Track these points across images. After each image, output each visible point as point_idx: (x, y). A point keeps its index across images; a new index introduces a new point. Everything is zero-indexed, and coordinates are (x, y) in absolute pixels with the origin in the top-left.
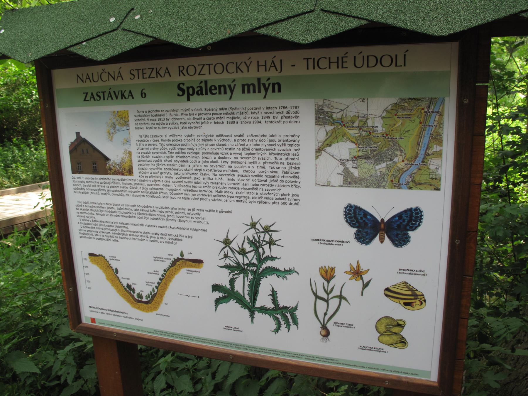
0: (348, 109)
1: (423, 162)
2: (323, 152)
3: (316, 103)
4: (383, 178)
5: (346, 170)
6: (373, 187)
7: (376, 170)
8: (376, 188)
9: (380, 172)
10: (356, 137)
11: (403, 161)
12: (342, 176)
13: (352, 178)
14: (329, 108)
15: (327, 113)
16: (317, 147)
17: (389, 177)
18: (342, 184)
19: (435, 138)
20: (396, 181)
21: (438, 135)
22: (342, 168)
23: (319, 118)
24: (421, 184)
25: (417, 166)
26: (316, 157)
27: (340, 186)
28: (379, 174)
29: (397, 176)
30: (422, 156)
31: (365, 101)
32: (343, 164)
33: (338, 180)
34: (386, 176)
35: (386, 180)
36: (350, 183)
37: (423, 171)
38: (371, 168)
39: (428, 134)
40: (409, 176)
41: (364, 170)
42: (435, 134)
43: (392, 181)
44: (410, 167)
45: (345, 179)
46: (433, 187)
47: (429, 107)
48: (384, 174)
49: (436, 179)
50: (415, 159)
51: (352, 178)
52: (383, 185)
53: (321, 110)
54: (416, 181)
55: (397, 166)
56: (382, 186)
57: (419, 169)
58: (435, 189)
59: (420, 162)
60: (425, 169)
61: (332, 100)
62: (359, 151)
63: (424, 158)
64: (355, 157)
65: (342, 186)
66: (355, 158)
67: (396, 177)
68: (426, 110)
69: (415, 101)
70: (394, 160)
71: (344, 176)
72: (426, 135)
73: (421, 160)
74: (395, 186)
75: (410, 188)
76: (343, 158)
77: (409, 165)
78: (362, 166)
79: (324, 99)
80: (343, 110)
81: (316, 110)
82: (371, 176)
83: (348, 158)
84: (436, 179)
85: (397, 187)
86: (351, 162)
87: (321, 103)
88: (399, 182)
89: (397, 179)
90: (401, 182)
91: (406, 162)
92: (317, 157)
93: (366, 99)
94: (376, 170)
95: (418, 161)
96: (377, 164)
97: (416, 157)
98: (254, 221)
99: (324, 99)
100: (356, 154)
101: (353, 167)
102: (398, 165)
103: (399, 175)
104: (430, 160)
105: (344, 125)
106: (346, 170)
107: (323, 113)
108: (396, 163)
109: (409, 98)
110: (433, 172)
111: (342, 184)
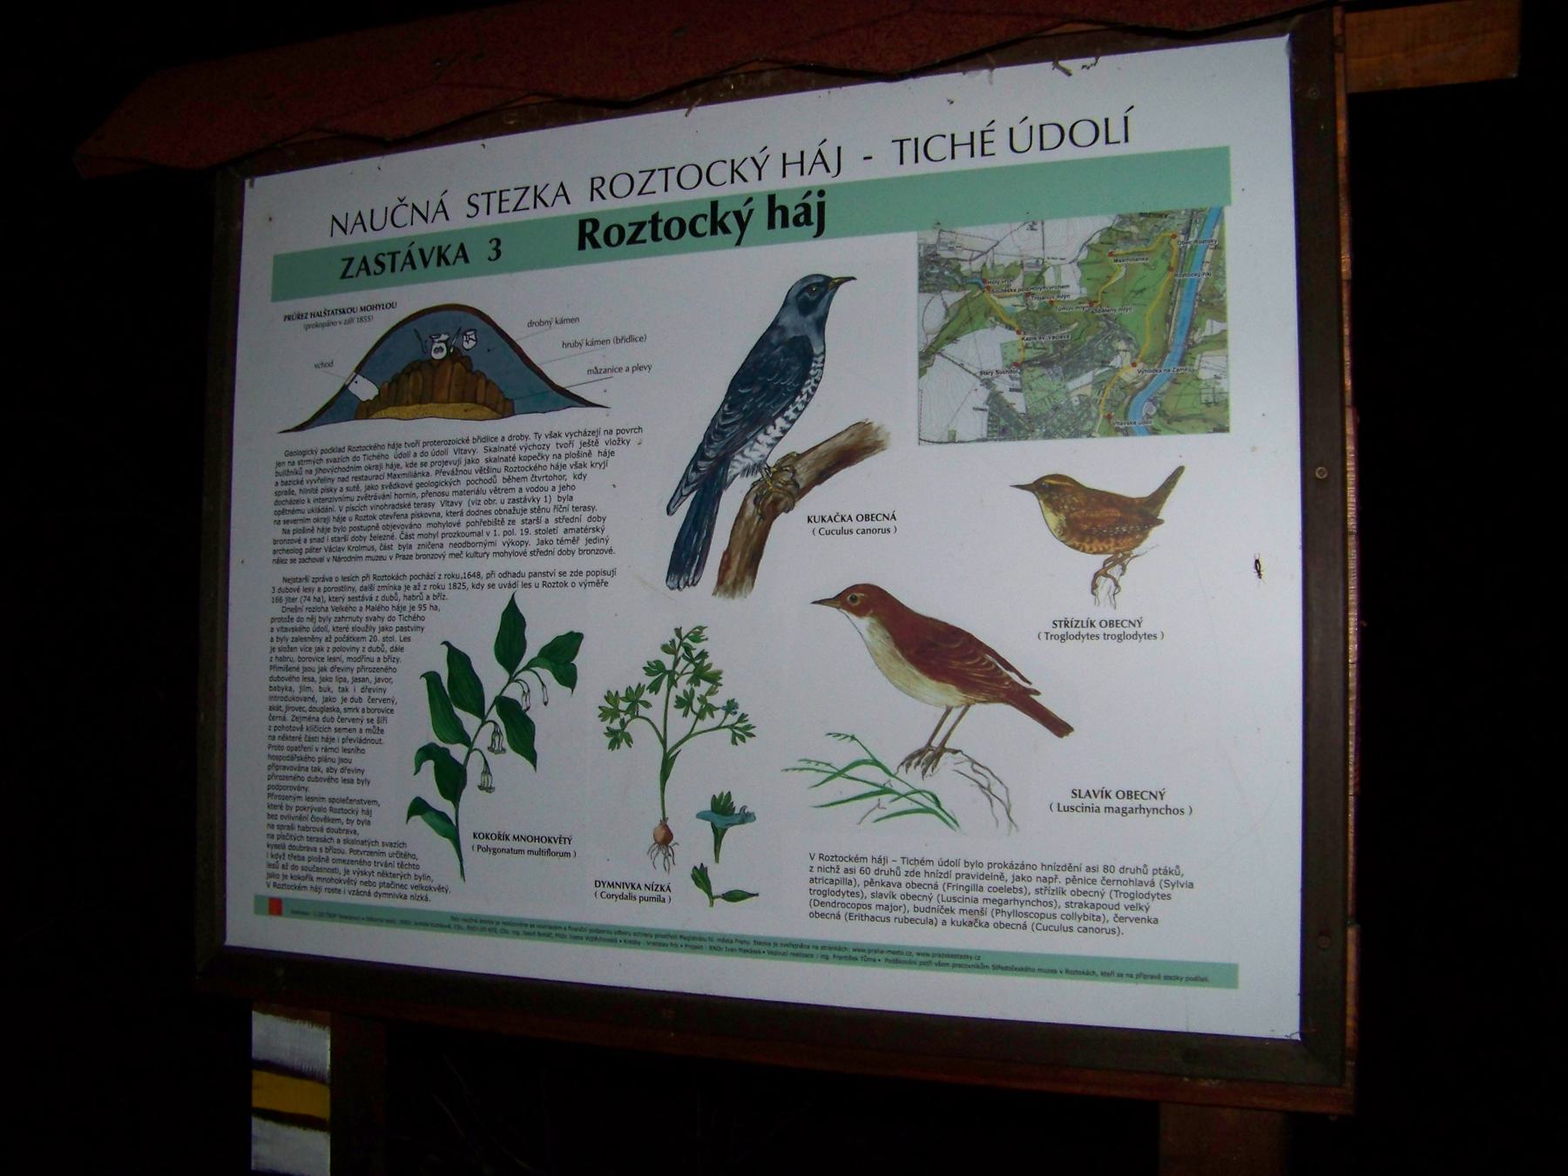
5: (995, 398)
7: (1068, 393)
11: (1134, 365)
14: (951, 249)
15: (948, 261)
16: (923, 348)
22: (984, 393)
28: (1075, 402)
30: (1180, 350)
31: (1038, 226)
32: (987, 384)
34: (1093, 408)
41: (1040, 395)
45: (993, 422)
48: (1088, 401)
49: (1216, 404)
50: (1163, 357)
52: (1086, 428)
57: (1175, 382)
58: (1215, 430)
64: (1016, 364)
65: (984, 440)
67: (1117, 407)
68: (1182, 238)
73: (1177, 358)
74: (1117, 430)
78: (1033, 385)
83: (1000, 368)
86: (1006, 377)
87: (931, 238)
89: (1122, 409)
91: (1140, 366)
100: (1019, 356)
102: (1122, 375)
106: (995, 398)
107: (937, 262)
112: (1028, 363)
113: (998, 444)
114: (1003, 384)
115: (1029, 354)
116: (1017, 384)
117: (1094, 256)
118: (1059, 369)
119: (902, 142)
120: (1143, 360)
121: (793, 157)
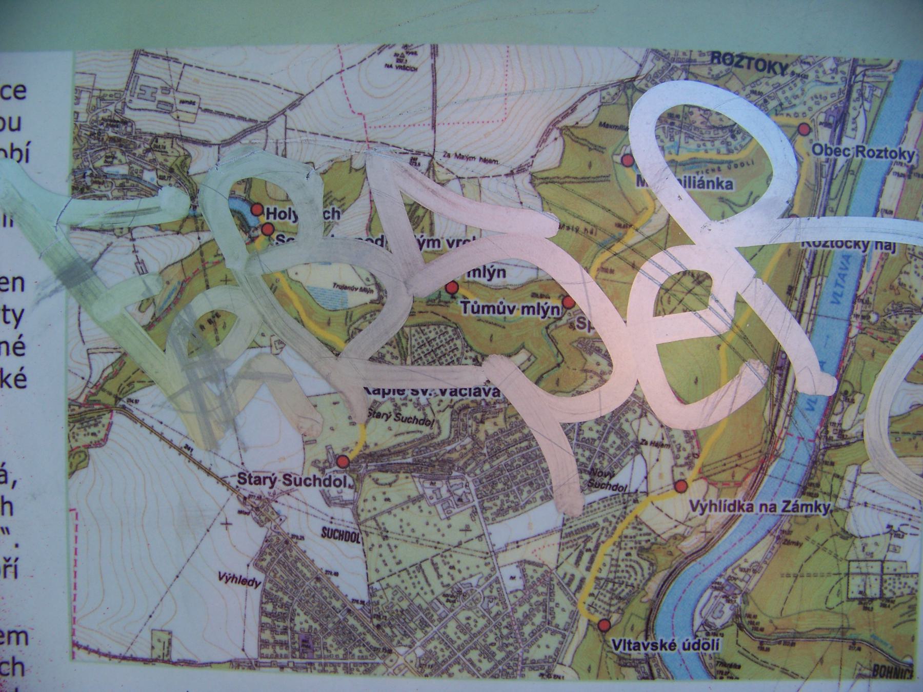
0: (296, 117)
1: (807, 487)
2: (119, 419)
3: (87, 82)
4: (546, 607)
5: (280, 550)
6: (473, 671)
7: (492, 554)
8: (492, 674)
9: (522, 563)
10: (349, 315)
11: (680, 486)
12: (255, 594)
13: (322, 612)
14: (166, 108)
15: (155, 143)
16: (76, 388)
17: (583, 597)
18: (253, 652)
19: (884, 327)
20: (628, 627)
21: (898, 309)
22: (249, 536)
23: (100, 178)
24: (790, 640)
25: (770, 520)
26: (72, 453)
27: (236, 664)
28: (508, 572)
29: (636, 590)
30: (804, 455)
31: (422, 60)
32: (258, 510)
33: (234, 621)
34: (560, 597)
35: (561, 619)
36: (306, 644)
37: (808, 548)
38: (454, 537)
39: (836, 298)
40: (716, 586)
41: (410, 554)
42: (881, 301)
43: (604, 627)
44: (727, 525)
45: (275, 615)
46: (863, 658)
47: (839, 121)
48: (547, 579)
49: (887, 602)
50: (761, 469)
51: (322, 612)
52: (537, 653)
53: (112, 123)
54: (763, 621)
55: (639, 523)
56: (534, 665)
57: (784, 539)
58: (878, 672)
59: (789, 492)
60: (819, 537)
61: (186, 55)
62: (374, 413)
63: (815, 462)
64: (341, 461)
65: (253, 665)
66: (346, 469)
67: (628, 600)
68: (824, 136)
69: (754, 75)
70: (621, 478)
71: (267, 596)
72: (826, 307)
73: (797, 474)
74: (624, 662)
75: (725, 670)
76: (253, 466)
77: (721, 516)
78: (391, 523)
79: (138, 54)
80: (266, 125)
81: (78, 126)
82: (455, 595)
83: (295, 467)
84: (887, 602)
85: (634, 664)
86: (312, 494)
87: (113, 78)
88: (648, 629)
89: (639, 608)
90: (662, 634)
91: (697, 490)
92: (78, 459)
93: (424, 52)
94: (492, 554)
95: (780, 484)
96: (502, 512)
97: (768, 455)
98: (596, 249)
99: (138, 54)
100: (350, 438)
101: (327, 533)
102: (646, 512)
103: (653, 586)
104: (851, 472)
105: (268, 230)
106: (280, 550)
107: (125, 146)
108: (628, 497)
109: (716, 57)
110: (870, 558)
111: (253, 652)
112: (379, 459)
113: (289, 676)
114: (304, 514)
115: (381, 435)
116: (344, 518)
117: (576, 164)
118: (465, 485)
119: (75, 644)
120: (703, 475)
121: (272, 210)
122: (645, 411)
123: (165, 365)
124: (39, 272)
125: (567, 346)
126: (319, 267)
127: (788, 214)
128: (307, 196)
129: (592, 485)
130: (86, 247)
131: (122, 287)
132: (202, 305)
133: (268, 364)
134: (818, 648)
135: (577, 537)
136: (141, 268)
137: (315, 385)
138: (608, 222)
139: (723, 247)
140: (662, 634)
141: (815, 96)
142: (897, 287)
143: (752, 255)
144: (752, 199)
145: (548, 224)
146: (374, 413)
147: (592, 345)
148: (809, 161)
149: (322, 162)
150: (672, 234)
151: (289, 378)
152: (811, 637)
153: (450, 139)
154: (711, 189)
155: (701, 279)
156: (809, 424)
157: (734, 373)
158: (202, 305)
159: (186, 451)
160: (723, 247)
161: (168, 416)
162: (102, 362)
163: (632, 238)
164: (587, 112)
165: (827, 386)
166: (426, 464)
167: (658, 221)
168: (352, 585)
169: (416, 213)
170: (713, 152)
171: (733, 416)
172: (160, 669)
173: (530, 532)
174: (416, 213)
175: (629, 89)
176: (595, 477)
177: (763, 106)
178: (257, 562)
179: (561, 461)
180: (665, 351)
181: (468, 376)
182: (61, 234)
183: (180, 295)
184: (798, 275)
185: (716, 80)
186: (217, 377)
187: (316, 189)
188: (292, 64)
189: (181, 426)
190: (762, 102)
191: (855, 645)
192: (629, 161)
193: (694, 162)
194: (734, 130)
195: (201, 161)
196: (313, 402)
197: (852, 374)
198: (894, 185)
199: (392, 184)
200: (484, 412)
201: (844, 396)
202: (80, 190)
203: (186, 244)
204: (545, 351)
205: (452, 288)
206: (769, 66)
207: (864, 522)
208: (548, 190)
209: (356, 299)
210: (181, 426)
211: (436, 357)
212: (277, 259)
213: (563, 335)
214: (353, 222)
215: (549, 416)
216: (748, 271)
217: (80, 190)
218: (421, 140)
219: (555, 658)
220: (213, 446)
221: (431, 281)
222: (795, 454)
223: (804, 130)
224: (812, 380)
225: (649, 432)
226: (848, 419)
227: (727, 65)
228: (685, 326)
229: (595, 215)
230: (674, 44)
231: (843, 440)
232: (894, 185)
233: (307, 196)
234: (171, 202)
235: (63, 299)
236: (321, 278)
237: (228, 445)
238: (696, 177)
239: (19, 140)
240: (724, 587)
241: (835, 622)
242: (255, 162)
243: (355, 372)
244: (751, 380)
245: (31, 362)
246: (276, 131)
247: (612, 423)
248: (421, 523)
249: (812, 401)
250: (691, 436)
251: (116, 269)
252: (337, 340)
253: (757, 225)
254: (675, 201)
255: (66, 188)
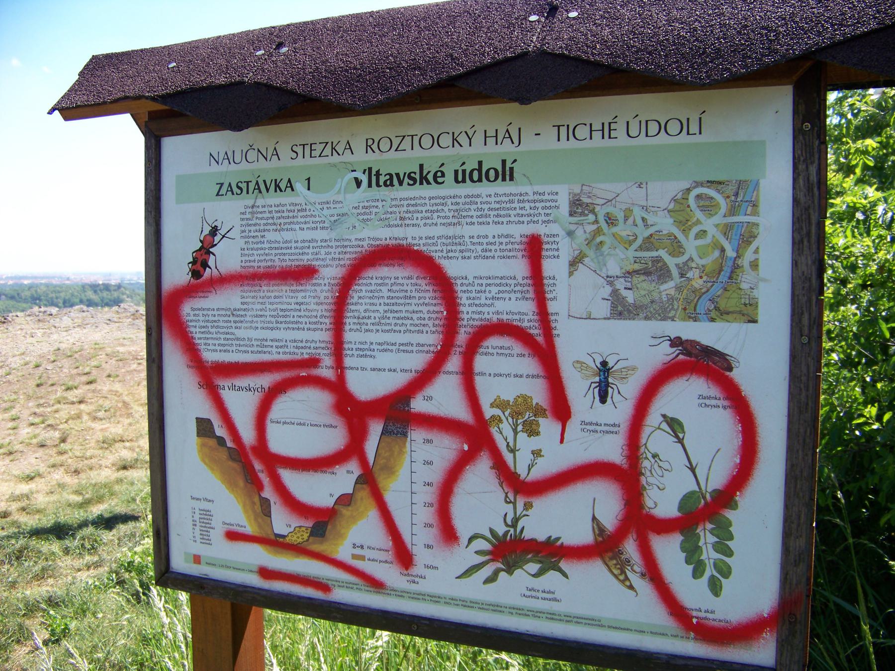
1: (730, 278)
5: (615, 293)
6: (657, 320)
7: (660, 292)
8: (661, 320)
11: (701, 277)
13: (624, 306)
14: (589, 197)
16: (571, 258)
20: (690, 309)
21: (751, 237)
22: (608, 289)
23: (575, 212)
24: (728, 313)
27: (605, 319)
29: (692, 301)
30: (729, 270)
31: (644, 186)
32: (611, 284)
33: (604, 308)
35: (676, 307)
36: (620, 314)
38: (652, 289)
41: (643, 293)
42: (746, 235)
43: (685, 309)
45: (614, 307)
47: (736, 195)
49: (751, 305)
50: (719, 273)
51: (624, 306)
52: (670, 315)
55: (692, 285)
56: (670, 318)
57: (725, 290)
58: (750, 321)
59: (726, 279)
61: (593, 185)
62: (635, 262)
63: (732, 272)
64: (628, 273)
65: (609, 319)
66: (630, 274)
68: (733, 198)
71: (612, 303)
72: (734, 237)
73: (728, 274)
74: (690, 317)
76: (610, 274)
77: (710, 284)
78: (639, 286)
82: (652, 302)
83: (618, 274)
84: (751, 305)
85: (692, 318)
86: (622, 280)
88: (695, 310)
89: (693, 305)
90: (698, 311)
91: (705, 278)
92: (571, 274)
94: (660, 292)
95: (724, 277)
97: (721, 270)
100: (630, 268)
101: (625, 288)
102: (693, 283)
105: (612, 223)
106: (615, 293)
108: (689, 280)
112: (636, 272)
114: (620, 284)
115: (637, 267)
117: (677, 208)
120: (706, 275)
122: (693, 261)
123: (591, 253)
124: (562, 233)
125: (677, 248)
126: (622, 230)
127: (725, 216)
128: (620, 216)
129: (682, 277)
130: (573, 227)
131: (581, 235)
132: (598, 240)
133: (613, 252)
134: (735, 315)
135: (679, 288)
136: (585, 232)
137: (623, 256)
138: (684, 220)
139: (711, 224)
140: (698, 311)
141: (730, 190)
142: (751, 232)
143: (717, 226)
144: (716, 213)
145: (671, 221)
146: (635, 262)
147: (681, 247)
148: (729, 204)
149: (623, 208)
150: (698, 222)
151: (617, 255)
152: (733, 312)
153: (650, 203)
154: (621, 139)
155: (705, 231)
156: (730, 263)
157: (713, 252)
158: (598, 240)
159: (595, 271)
160: (711, 224)
161: (591, 264)
162: (577, 252)
163: (690, 223)
164: (679, 196)
165: (734, 255)
166: (647, 273)
167: (695, 219)
168: (630, 300)
169: (643, 219)
170: (707, 203)
171: (713, 262)
172: (588, 320)
173: (668, 287)
174: (643, 219)
175: (688, 190)
176: (682, 275)
177: (719, 192)
178: (610, 295)
179: (675, 272)
180: (697, 247)
181: (654, 254)
182: (567, 224)
183: (594, 237)
184: (727, 230)
185: (708, 187)
186: (602, 255)
187: (622, 214)
188: (617, 187)
189: (593, 265)
190: (718, 191)
191: (743, 315)
192: (689, 206)
193: (703, 206)
194: (712, 198)
195: (597, 209)
196: (622, 260)
197: (740, 252)
198: (750, 208)
199: (638, 213)
200: (658, 261)
201: (738, 257)
202: (571, 215)
203: (595, 227)
204: (671, 249)
205: (651, 235)
206: (720, 183)
207: (744, 286)
208: (672, 213)
209: (631, 238)
210: (593, 265)
211: (648, 250)
212: (614, 230)
213: (675, 244)
214: (630, 221)
215: (672, 262)
216: (715, 229)
217: (571, 215)
218: (644, 203)
219: (674, 316)
220: (601, 270)
221: (647, 234)
222: (727, 270)
223: (728, 197)
224: (730, 253)
225: (694, 265)
226: (739, 262)
227: (710, 183)
228: (700, 242)
229: (681, 218)
230: (698, 179)
231: (738, 267)
232: (750, 208)
233: (620, 216)
234: (591, 217)
235: (567, 239)
236: (624, 234)
237: (604, 270)
238: (703, 209)
239: (557, 204)
240: (712, 300)
241: (738, 309)
242: (609, 209)
243: (631, 253)
244: (717, 253)
245: (560, 253)
246: (613, 202)
247: (685, 264)
248: (644, 285)
249: (731, 259)
250: (703, 266)
251: (579, 232)
252: (627, 246)
253: (718, 219)
254: (699, 215)
255: (568, 214)
